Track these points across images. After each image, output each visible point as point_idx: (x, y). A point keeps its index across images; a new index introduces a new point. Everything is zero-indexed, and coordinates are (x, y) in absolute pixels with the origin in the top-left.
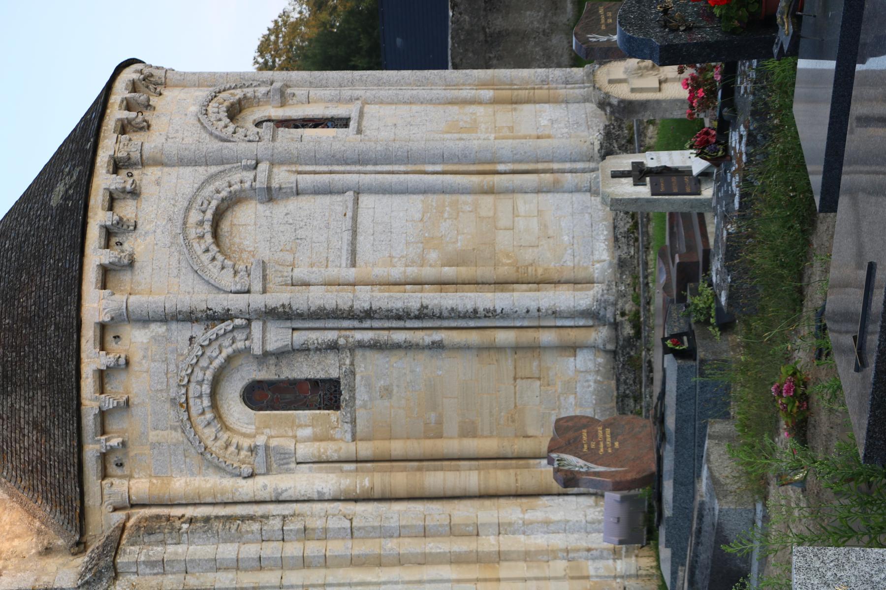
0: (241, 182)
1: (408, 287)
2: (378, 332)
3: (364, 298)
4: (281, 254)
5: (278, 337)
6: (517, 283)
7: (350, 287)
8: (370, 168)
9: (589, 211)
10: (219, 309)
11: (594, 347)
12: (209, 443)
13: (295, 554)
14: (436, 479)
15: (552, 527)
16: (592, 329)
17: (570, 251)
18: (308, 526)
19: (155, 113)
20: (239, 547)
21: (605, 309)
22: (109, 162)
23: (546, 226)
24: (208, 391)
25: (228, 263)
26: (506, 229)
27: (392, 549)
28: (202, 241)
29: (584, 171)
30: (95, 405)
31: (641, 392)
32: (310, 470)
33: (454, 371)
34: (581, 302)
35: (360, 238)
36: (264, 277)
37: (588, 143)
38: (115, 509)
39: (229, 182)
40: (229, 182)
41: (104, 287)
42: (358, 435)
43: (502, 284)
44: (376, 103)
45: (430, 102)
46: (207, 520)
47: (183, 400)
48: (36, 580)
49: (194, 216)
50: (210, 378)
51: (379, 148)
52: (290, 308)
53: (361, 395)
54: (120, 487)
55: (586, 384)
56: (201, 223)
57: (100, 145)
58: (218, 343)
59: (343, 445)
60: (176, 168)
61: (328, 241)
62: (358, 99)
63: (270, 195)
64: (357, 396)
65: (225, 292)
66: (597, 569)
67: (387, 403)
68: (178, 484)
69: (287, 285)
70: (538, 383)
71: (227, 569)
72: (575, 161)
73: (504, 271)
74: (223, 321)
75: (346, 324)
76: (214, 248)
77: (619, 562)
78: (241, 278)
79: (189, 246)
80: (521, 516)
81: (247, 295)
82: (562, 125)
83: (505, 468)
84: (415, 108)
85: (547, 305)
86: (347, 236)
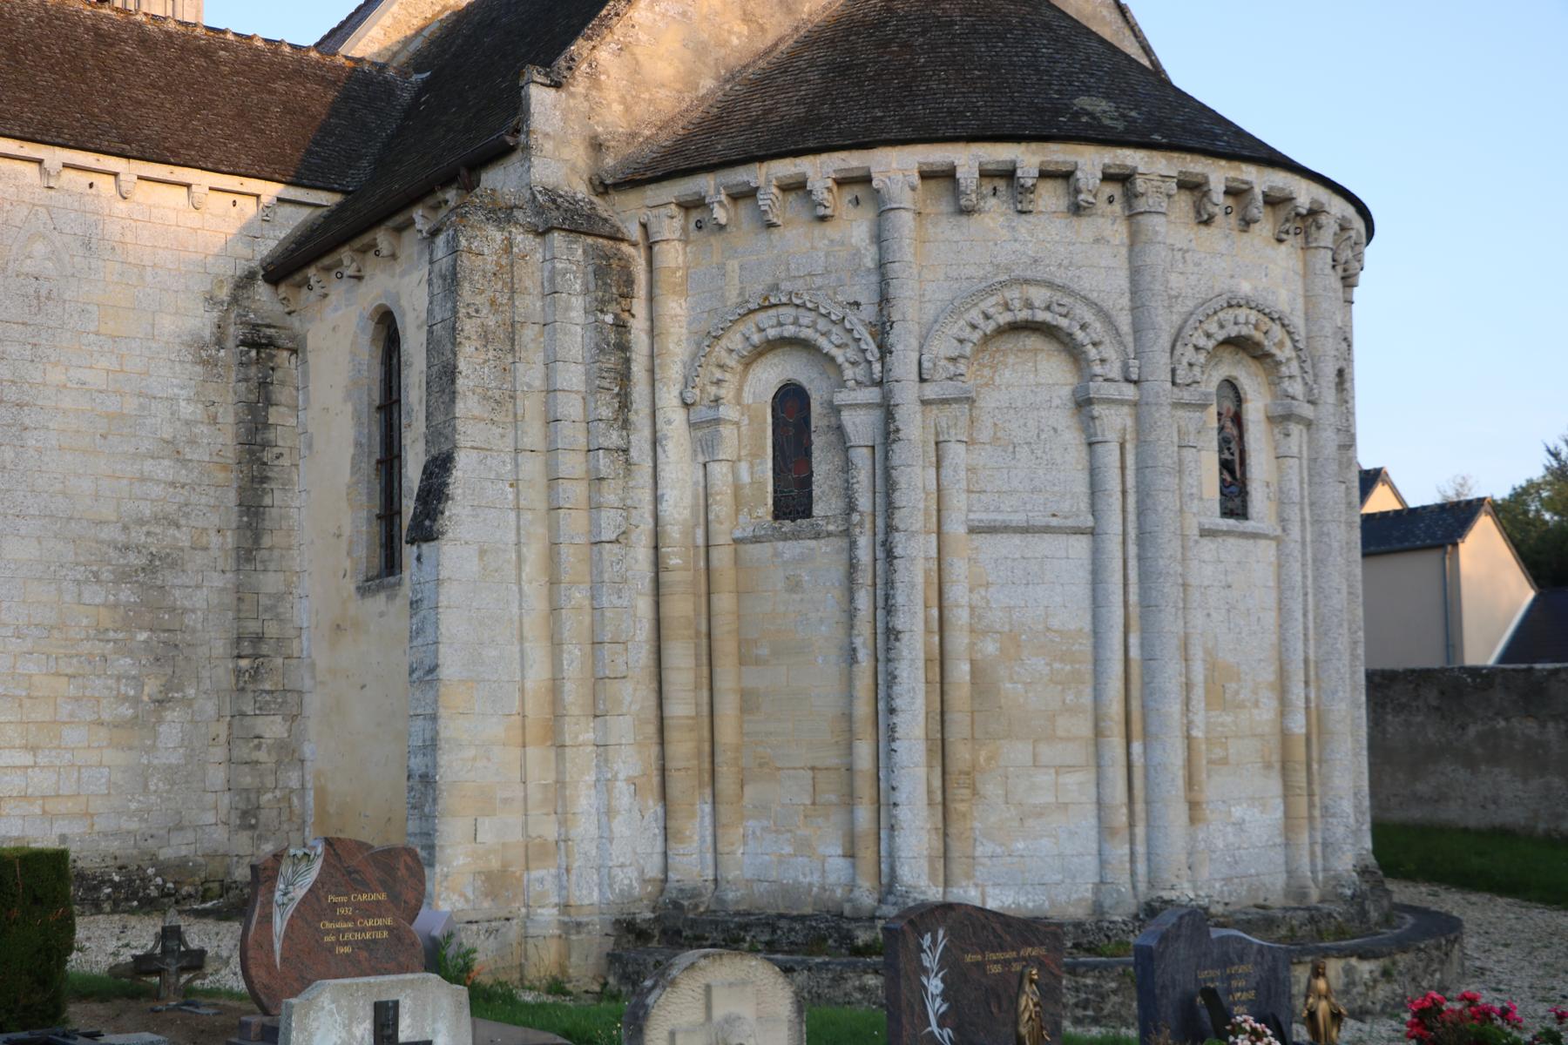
0: (1103, 361)
1: (935, 612)
2: (870, 569)
3: (915, 551)
4: (989, 424)
5: (861, 425)
6: (944, 773)
7: (934, 527)
8: (1133, 550)
9: (1068, 881)
10: (892, 339)
11: (852, 886)
12: (724, 342)
13: (562, 468)
14: (681, 657)
15: (604, 819)
16: (876, 884)
17: (999, 850)
18: (605, 483)
19: (1235, 233)
20: (577, 392)
21: (895, 904)
22: (1126, 166)
23: (1040, 815)
24: (786, 334)
25: (968, 349)
26: (1035, 756)
27: (569, 598)
28: (1001, 309)
29: (1133, 873)
30: (761, 181)
31: (777, 952)
32: (696, 483)
33: (820, 679)
34: (906, 868)
35: (1017, 539)
36: (945, 401)
37: (1174, 881)
38: (644, 226)
39: (1100, 343)
40: (1100, 343)
41: (926, 176)
42: (742, 547)
43: (941, 749)
44: (1278, 558)
45: (1282, 639)
46: (623, 347)
47: (773, 300)
48: (546, 135)
49: (1039, 295)
50: (802, 335)
51: (1161, 562)
52: (894, 441)
53: (790, 549)
54: (670, 226)
55: (807, 870)
56: (1029, 305)
57: (1154, 153)
58: (850, 342)
59: (726, 527)
60: (1126, 265)
61: (1012, 492)
62: (1284, 530)
63: (1083, 403)
64: (789, 544)
65: (921, 346)
66: (542, 881)
67: (780, 585)
68: (674, 305)
69: (937, 434)
70: (808, 802)
71: (547, 377)
72: (1149, 860)
73: (961, 754)
74: (880, 347)
75: (880, 522)
76: (990, 327)
77: (555, 911)
78: (945, 369)
79: (991, 290)
80: (621, 776)
81: (915, 376)
82: (1231, 838)
83: (699, 754)
84: (1270, 618)
85: (901, 817)
86: (1018, 519)
